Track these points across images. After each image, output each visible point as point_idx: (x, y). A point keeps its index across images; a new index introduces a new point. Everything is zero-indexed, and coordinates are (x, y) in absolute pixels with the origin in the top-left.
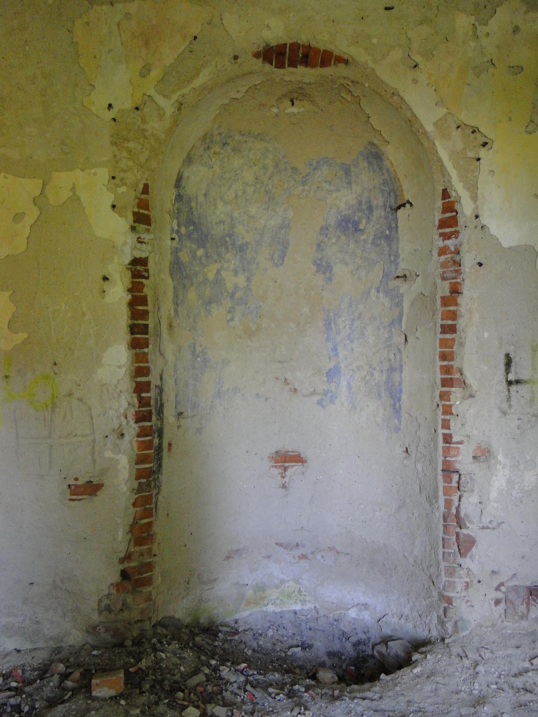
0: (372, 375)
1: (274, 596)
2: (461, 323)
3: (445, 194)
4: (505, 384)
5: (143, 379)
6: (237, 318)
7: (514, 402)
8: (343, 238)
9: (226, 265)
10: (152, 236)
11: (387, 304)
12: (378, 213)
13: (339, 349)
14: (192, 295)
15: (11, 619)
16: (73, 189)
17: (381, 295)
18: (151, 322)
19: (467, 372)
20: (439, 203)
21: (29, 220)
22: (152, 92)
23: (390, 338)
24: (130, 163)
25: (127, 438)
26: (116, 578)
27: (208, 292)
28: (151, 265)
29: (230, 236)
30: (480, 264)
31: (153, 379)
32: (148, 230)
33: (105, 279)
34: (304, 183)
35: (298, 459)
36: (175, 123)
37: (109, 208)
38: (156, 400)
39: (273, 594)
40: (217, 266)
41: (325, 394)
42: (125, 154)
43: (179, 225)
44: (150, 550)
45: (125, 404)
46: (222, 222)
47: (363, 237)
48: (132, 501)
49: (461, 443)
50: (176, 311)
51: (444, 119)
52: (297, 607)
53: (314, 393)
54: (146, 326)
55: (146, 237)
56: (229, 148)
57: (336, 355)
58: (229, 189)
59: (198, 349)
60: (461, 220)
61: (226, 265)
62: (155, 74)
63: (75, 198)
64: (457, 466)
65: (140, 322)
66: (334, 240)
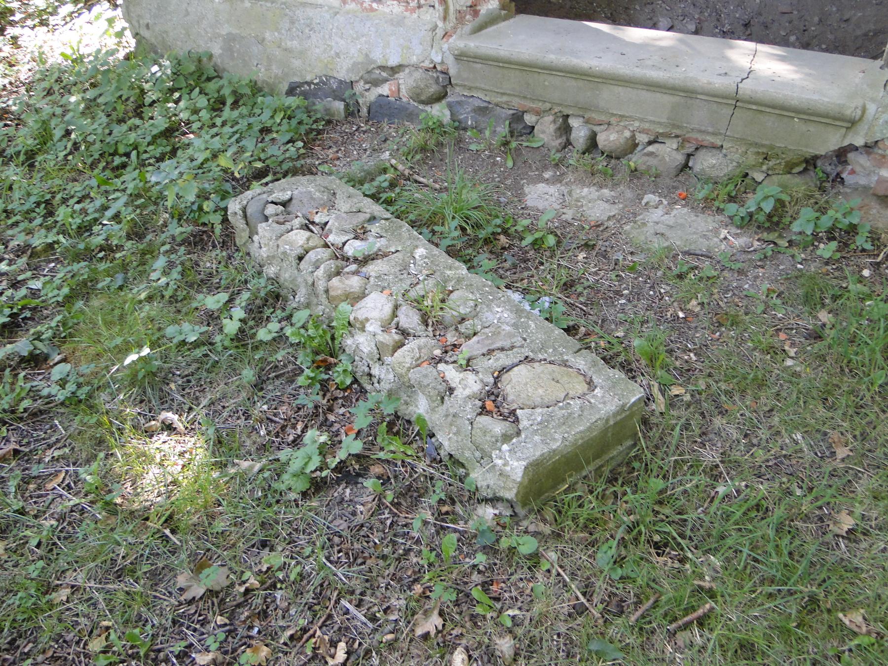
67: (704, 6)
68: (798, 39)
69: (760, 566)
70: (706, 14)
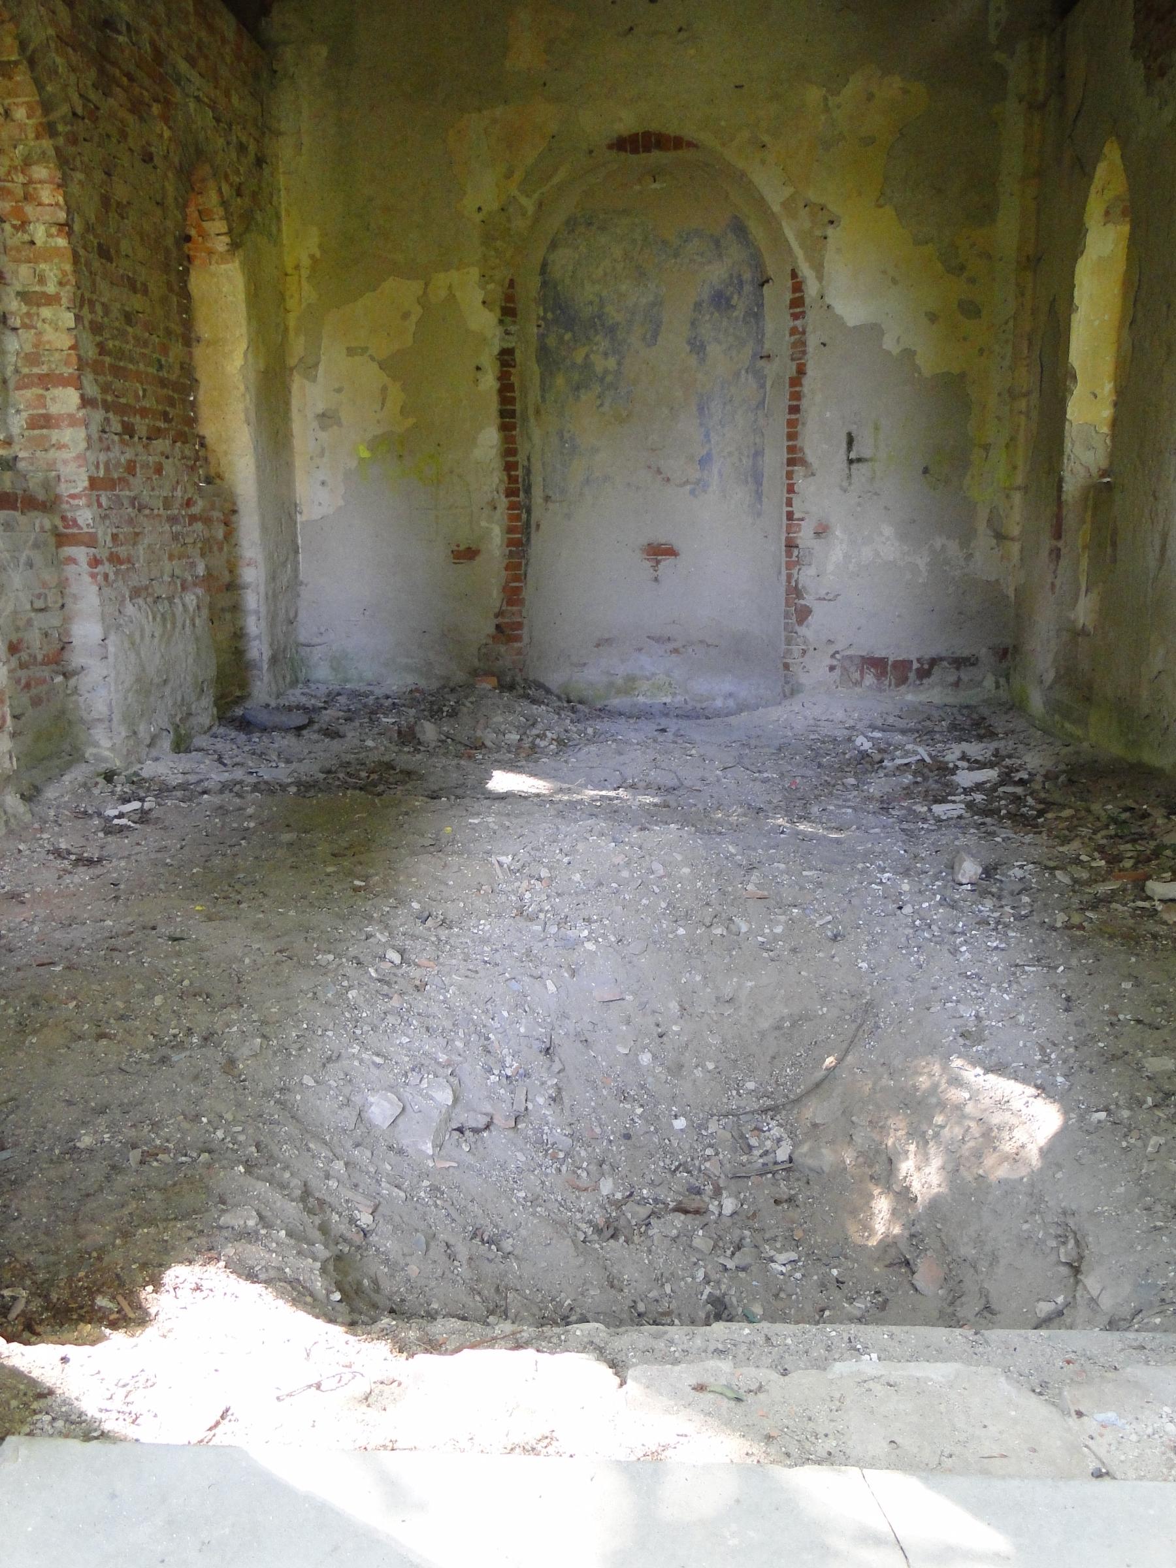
0: (740, 460)
1: (645, 688)
2: (804, 404)
3: (794, 274)
4: (845, 463)
5: (511, 459)
6: (607, 404)
7: (855, 479)
8: (716, 314)
9: (595, 348)
10: (518, 327)
11: (755, 386)
12: (748, 288)
13: (712, 434)
14: (560, 381)
15: (410, 661)
16: (450, 287)
17: (750, 376)
18: (518, 407)
19: (807, 451)
20: (789, 283)
21: (414, 319)
22: (516, 193)
23: (755, 421)
24: (498, 261)
25: (499, 511)
26: (491, 630)
27: (576, 377)
28: (518, 355)
29: (600, 317)
30: (824, 345)
31: (521, 458)
32: (514, 322)
33: (478, 368)
34: (676, 256)
35: (671, 552)
36: (536, 220)
37: (480, 305)
38: (524, 480)
39: (645, 686)
40: (587, 349)
41: (698, 482)
42: (493, 253)
43: (545, 311)
44: (520, 612)
45: (497, 480)
46: (591, 303)
47: (735, 314)
48: (504, 565)
49: (802, 520)
50: (543, 397)
51: (792, 198)
52: (668, 700)
53: (687, 482)
54: (514, 411)
55: (513, 329)
56: (594, 228)
57: (709, 441)
58: (597, 267)
59: (566, 435)
60: (807, 301)
61: (595, 348)
62: (518, 175)
63: (451, 297)
64: (799, 542)
65: (509, 407)
66: (707, 317)
67: (448, 1024)
68: (655, 1057)
69: (1109, 550)
70: (459, 1044)
